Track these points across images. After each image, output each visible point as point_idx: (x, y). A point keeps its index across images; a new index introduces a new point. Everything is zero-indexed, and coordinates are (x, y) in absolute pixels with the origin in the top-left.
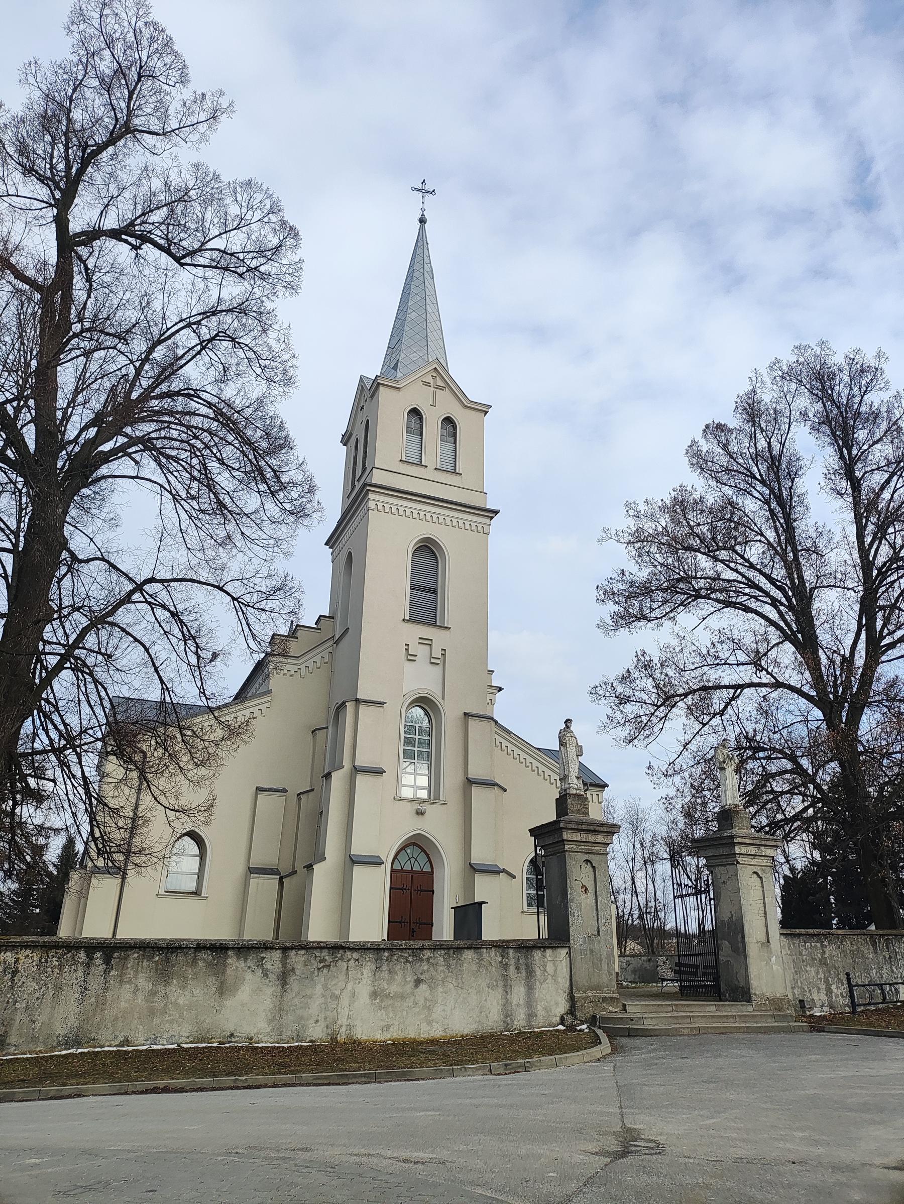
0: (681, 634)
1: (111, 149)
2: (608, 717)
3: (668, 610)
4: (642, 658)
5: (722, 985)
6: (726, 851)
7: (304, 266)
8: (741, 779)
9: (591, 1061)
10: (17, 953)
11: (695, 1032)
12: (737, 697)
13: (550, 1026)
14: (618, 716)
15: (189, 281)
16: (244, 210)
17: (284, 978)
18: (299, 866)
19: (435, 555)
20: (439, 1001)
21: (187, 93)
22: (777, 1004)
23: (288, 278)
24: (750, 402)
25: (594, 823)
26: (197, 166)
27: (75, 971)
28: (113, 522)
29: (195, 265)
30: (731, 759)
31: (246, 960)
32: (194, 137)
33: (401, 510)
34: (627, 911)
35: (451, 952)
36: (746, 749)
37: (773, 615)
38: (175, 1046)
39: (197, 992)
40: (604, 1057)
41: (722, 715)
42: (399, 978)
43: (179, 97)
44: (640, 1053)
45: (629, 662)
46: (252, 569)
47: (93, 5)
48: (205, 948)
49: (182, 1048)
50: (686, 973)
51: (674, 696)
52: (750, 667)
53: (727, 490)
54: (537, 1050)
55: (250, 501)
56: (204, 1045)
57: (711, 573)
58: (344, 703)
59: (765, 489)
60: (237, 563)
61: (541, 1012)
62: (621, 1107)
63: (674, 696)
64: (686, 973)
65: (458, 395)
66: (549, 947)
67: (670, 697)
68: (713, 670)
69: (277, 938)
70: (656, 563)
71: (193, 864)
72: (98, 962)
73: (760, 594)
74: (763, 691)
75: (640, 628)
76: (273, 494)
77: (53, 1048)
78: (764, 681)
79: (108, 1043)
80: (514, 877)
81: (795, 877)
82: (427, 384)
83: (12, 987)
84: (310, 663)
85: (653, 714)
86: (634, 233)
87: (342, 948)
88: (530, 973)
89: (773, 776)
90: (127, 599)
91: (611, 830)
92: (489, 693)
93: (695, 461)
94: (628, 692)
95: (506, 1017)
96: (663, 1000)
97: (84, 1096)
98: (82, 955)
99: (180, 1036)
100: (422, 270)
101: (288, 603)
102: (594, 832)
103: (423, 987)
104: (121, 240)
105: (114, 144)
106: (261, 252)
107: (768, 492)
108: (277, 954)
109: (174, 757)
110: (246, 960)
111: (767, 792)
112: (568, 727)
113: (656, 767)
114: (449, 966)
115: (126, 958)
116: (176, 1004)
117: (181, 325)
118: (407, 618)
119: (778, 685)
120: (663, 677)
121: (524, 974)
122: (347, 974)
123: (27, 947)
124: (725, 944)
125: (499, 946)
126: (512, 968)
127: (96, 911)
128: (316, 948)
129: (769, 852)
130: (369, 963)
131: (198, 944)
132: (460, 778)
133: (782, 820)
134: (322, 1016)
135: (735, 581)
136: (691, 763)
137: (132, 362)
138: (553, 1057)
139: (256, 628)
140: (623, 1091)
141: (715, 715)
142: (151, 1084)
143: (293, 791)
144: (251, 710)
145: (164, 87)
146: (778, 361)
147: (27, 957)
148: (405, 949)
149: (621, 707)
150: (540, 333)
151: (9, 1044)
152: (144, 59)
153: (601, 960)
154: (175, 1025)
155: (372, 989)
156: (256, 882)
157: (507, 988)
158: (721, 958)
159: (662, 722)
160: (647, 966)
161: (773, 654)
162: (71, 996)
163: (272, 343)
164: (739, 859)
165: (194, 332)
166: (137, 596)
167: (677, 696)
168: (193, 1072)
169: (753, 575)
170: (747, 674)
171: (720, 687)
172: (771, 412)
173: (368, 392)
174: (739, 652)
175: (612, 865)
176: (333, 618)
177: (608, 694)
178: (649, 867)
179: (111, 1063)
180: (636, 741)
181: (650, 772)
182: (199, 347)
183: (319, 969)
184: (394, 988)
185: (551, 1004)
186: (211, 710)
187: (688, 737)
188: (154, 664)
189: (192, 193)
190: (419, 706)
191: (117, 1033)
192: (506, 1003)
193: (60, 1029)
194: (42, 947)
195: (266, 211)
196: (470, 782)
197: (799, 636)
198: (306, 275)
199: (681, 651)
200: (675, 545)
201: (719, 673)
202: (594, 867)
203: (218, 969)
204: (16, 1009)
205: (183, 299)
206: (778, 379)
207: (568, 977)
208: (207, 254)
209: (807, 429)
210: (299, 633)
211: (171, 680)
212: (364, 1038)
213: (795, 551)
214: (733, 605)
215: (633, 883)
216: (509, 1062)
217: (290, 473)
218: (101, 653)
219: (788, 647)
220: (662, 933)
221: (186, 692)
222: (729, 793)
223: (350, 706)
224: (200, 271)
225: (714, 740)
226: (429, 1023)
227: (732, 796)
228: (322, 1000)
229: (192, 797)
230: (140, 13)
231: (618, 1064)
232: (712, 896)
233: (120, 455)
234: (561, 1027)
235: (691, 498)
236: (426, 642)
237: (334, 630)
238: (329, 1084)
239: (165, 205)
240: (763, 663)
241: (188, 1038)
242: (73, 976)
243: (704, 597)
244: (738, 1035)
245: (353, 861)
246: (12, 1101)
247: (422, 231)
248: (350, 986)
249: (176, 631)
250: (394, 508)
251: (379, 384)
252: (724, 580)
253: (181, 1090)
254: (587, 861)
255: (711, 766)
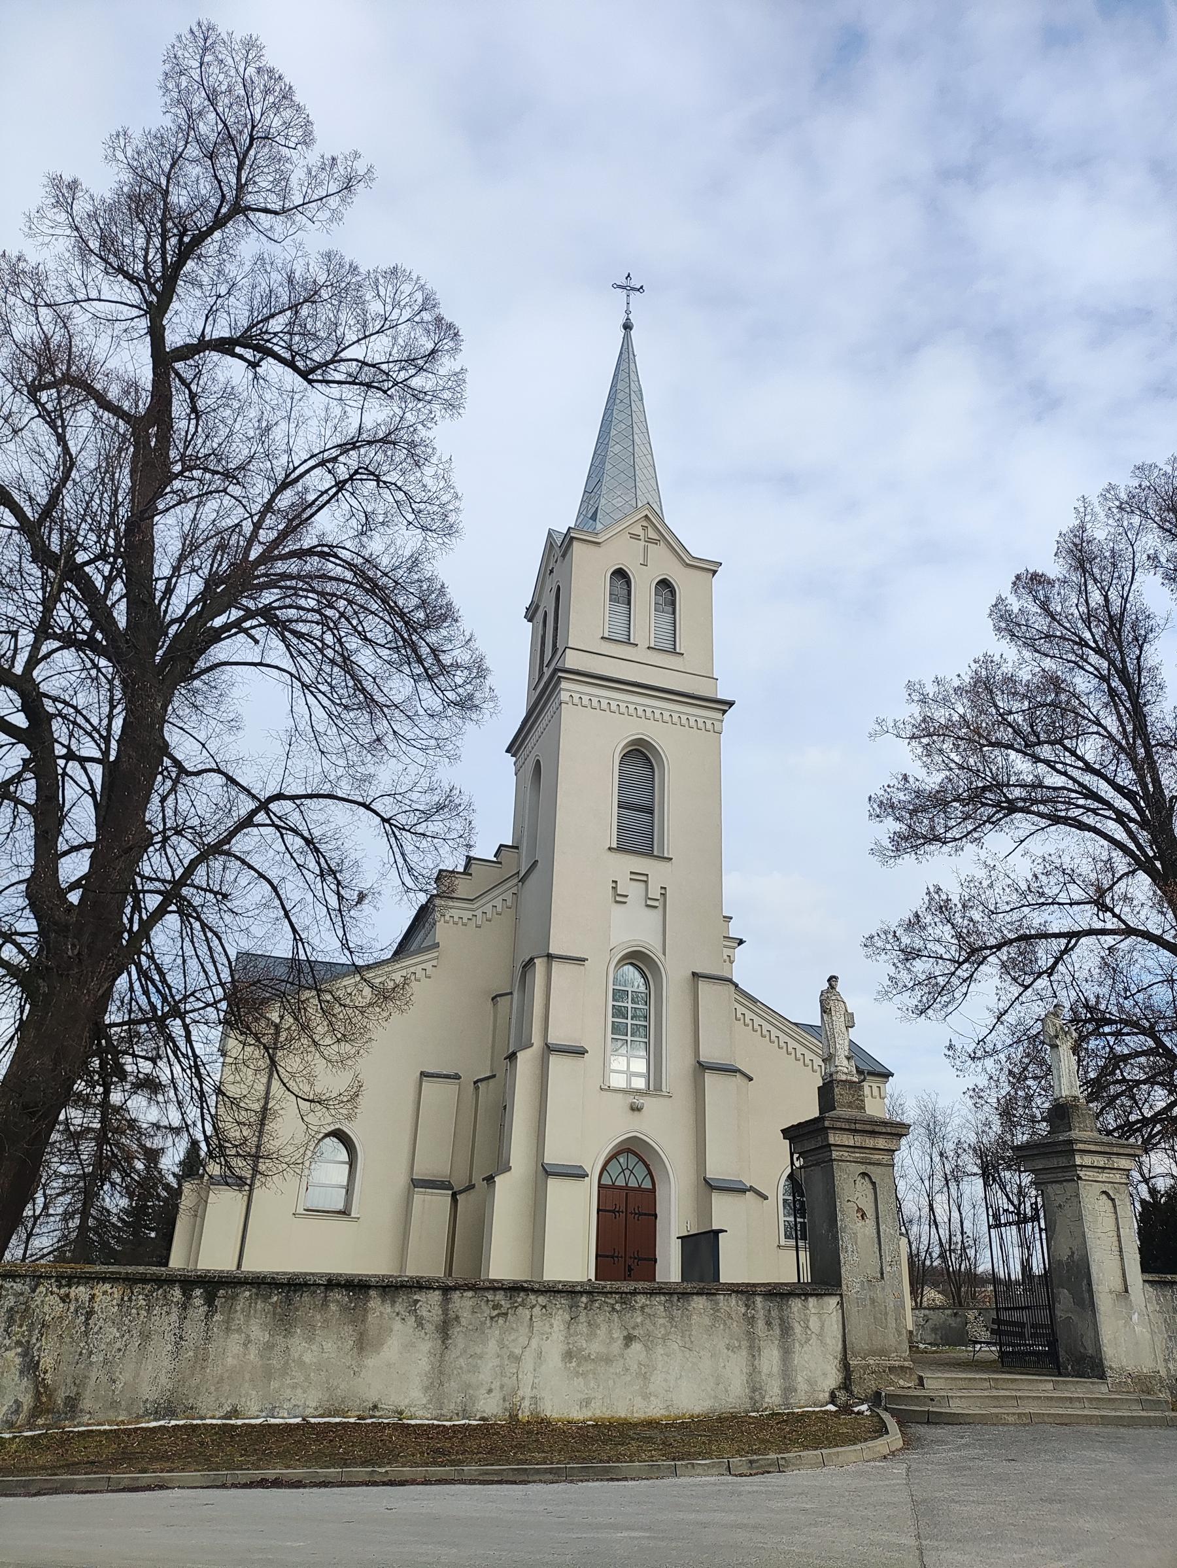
0: (990, 862)
1: (217, 235)
2: (891, 978)
3: (970, 828)
4: (936, 897)
5: (1062, 1353)
6: (1062, 1162)
7: (468, 377)
8: (1079, 1061)
9: (874, 1460)
10: (92, 1288)
11: (1025, 1421)
12: (1072, 949)
13: (815, 1405)
14: (905, 977)
15: (322, 406)
16: (389, 308)
17: (445, 1329)
18: (477, 1179)
19: (650, 762)
20: (660, 1366)
21: (312, 157)
22: (1143, 1384)
23: (446, 395)
24: (1077, 541)
25: (873, 1122)
26: (329, 256)
27: (168, 1313)
28: (234, 725)
29: (328, 382)
30: (1066, 1033)
31: (393, 1303)
32: (324, 215)
33: (604, 702)
34: (923, 1248)
35: (675, 1298)
36: (1086, 1021)
37: (1120, 835)
38: (298, 1420)
39: (329, 1346)
40: (893, 1453)
41: (1050, 975)
42: (602, 1332)
43: (302, 162)
44: (945, 1450)
45: (918, 902)
46: (407, 782)
47: (191, 50)
48: (338, 1285)
49: (308, 1423)
50: (1008, 1333)
51: (981, 949)
52: (1088, 907)
53: (1048, 663)
54: (795, 1441)
55: (399, 687)
56: (337, 1420)
57: (1029, 779)
58: (532, 959)
59: (1102, 661)
60: (386, 774)
61: (802, 1386)
62: (918, 1537)
63: (981, 949)
64: (1008, 1333)
65: (677, 550)
66: (812, 1295)
67: (977, 950)
68: (1036, 913)
69: (450, 1275)
70: (953, 765)
71: (340, 1174)
72: (198, 1302)
73: (1100, 806)
74: (1109, 940)
75: (931, 854)
76: (430, 678)
77: (138, 1418)
78: (1109, 926)
79: (210, 1414)
80: (766, 1198)
81: (1156, 1203)
82: (635, 537)
83: (86, 1333)
84: (488, 908)
85: (953, 974)
86: (911, 349)
87: (524, 1289)
88: (786, 1331)
89: (1125, 1058)
90: (248, 822)
91: (897, 1131)
92: (725, 946)
93: (1003, 625)
94: (918, 944)
95: (754, 1391)
96: (977, 1372)
97: (168, 1488)
98: (177, 1293)
99: (306, 1406)
100: (627, 390)
101: (454, 825)
102: (873, 1133)
103: (636, 1346)
104: (234, 355)
105: (220, 227)
106: (411, 361)
107: (1106, 664)
108: (436, 1296)
109: (305, 1028)
110: (393, 1303)
111: (1117, 1082)
112: (832, 987)
113: (959, 1047)
114: (672, 1318)
115: (234, 1298)
116: (301, 1363)
117: (311, 463)
118: (614, 845)
119: (1130, 931)
120: (966, 922)
121: (778, 1332)
122: (531, 1326)
123: (104, 1280)
124: (1064, 1295)
125: (742, 1292)
126: (761, 1324)
127: (213, 1237)
128: (487, 1289)
129: (1124, 1163)
130: (561, 1312)
131: (330, 1281)
132: (689, 1061)
133: (1138, 1121)
134: (496, 1385)
135: (1064, 788)
136: (1009, 1042)
137: (251, 516)
138: (818, 1452)
139: (413, 859)
140: (922, 1509)
141: (1040, 975)
142: (258, 1474)
143: (468, 1078)
144: (412, 969)
145: (285, 151)
146: (1111, 487)
147: (105, 1293)
148: (611, 1293)
149: (908, 965)
150: (788, 483)
151: (81, 1411)
152: (258, 117)
153: (886, 1314)
154: (299, 1391)
155: (566, 1347)
156: (422, 1198)
157: (754, 1351)
158: (1058, 1313)
159: (966, 984)
160: (953, 1322)
161: (1120, 888)
162: (162, 1347)
163: (429, 482)
164: (1081, 1174)
165: (330, 472)
166: (261, 817)
167: (986, 948)
168: (317, 1459)
169: (1088, 779)
170: (1086, 917)
171: (1046, 936)
172: (1108, 554)
173: (559, 550)
174: (1071, 887)
175: (901, 1185)
176: (517, 848)
177: (889, 947)
178: (953, 1185)
179: (212, 1441)
180: (930, 1012)
181: (951, 1053)
182: (334, 490)
183: (492, 1318)
184: (595, 1347)
185: (815, 1374)
186: (358, 969)
187: (1002, 1006)
188: (284, 908)
189: (325, 294)
190: (632, 964)
191: (223, 1400)
192: (754, 1372)
193: (148, 1392)
194: (124, 1280)
195: (416, 308)
196: (702, 1067)
197: (1158, 864)
198: (471, 390)
199: (991, 886)
200: (976, 738)
201: (1045, 916)
202: (874, 1184)
203: (356, 1316)
204: (91, 1363)
205: (315, 430)
206: (1115, 510)
207: (840, 1336)
208: (343, 367)
209: (1159, 578)
210: (474, 869)
211: (307, 928)
212: (555, 1415)
213: (1147, 746)
214: (1065, 821)
215: (931, 1208)
216: (755, 1457)
217: (455, 653)
218: (211, 891)
219: (1143, 878)
220: (973, 1278)
221: (325, 946)
222: (1064, 1080)
223: (540, 963)
224: (335, 390)
225: (1039, 1009)
226: (646, 1397)
227: (1068, 1082)
228: (497, 1362)
229: (330, 1082)
230: (250, 57)
231: (914, 1466)
232: (1043, 1226)
233: (234, 631)
234: (831, 1408)
235: (999, 672)
236: (641, 878)
237: (519, 865)
238: (500, 1482)
239: (290, 308)
240: (1108, 900)
241: (316, 1409)
242: (165, 1320)
243: (1022, 810)
244: (1088, 1428)
245: (548, 1172)
246: (72, 1492)
247: (627, 340)
248: (534, 1343)
249: (312, 865)
250: (595, 700)
251: (572, 538)
252: (1048, 788)
253: (298, 1484)
254: (864, 1175)
255: (1036, 1047)
